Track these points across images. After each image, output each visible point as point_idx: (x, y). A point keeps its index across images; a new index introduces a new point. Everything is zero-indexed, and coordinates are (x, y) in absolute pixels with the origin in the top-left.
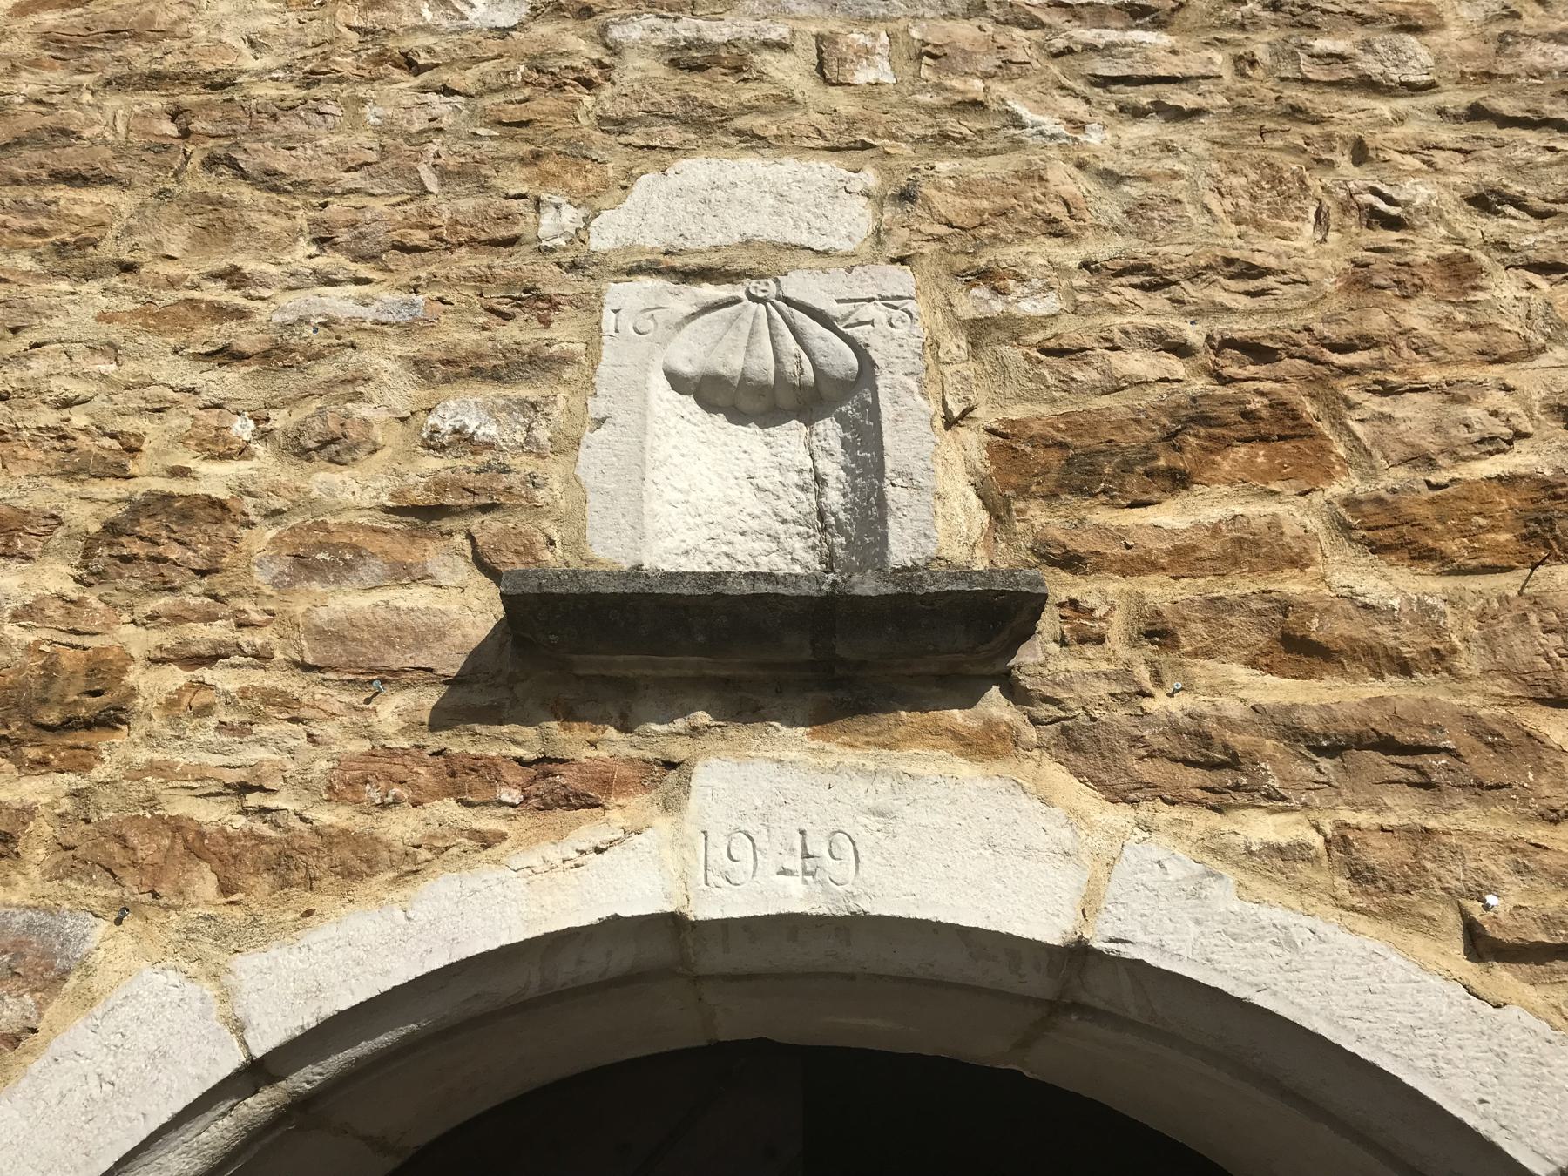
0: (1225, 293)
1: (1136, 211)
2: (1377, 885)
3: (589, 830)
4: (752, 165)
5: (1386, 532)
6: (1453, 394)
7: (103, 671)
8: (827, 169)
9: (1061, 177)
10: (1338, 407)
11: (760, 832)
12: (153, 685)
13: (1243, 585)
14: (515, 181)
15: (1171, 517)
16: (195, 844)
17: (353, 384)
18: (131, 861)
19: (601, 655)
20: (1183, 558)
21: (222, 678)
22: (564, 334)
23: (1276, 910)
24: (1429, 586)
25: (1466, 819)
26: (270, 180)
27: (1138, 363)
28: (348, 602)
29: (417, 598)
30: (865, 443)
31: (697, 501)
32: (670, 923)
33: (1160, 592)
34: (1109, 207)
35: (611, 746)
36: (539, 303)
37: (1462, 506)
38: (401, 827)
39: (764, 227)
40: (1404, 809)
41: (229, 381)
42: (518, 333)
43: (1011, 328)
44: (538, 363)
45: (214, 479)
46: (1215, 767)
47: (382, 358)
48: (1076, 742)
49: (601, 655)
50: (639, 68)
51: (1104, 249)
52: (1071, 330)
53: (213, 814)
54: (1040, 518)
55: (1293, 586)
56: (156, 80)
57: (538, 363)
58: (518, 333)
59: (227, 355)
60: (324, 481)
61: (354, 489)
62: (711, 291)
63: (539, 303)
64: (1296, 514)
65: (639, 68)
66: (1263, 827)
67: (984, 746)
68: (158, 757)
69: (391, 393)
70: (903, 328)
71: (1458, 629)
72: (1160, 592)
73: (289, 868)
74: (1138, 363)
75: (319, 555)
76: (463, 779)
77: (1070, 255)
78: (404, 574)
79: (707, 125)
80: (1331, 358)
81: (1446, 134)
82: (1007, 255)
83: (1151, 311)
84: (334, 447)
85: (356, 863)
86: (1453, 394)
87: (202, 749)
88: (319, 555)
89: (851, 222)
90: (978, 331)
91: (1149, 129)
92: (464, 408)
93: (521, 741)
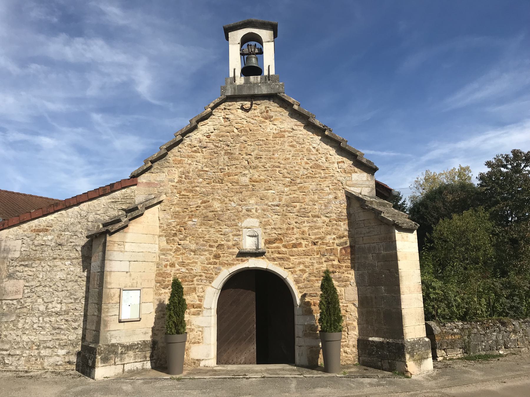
0: (279, 230)
1: (275, 224)
2: (280, 265)
3: (244, 263)
4: (252, 219)
5: (285, 246)
6: (291, 237)
7: (219, 254)
8: (256, 220)
9: (271, 221)
10: (284, 238)
11: (252, 263)
12: (222, 255)
13: (277, 250)
14: (237, 221)
15: (274, 245)
16: (226, 264)
17: (229, 236)
18: (223, 264)
19: (243, 255)
20: (274, 248)
21: (225, 255)
22: (241, 233)
23: (276, 267)
24: (286, 249)
25: (286, 262)
26: (221, 221)
27: (273, 235)
28: (231, 250)
29: (234, 250)
30: (258, 240)
31: (249, 244)
32: (231, 291)
33: (273, 250)
34: (273, 223)
35: (245, 258)
36: (239, 231)
37: (289, 245)
38: (235, 263)
39: (253, 225)
40: (283, 262)
41: (222, 236)
42: (238, 233)
43: (266, 232)
44: (239, 235)
45: (222, 243)
46: (274, 259)
47: (230, 234)
48: (268, 258)
49: (243, 255)
50: (244, 211)
51: (272, 227)
52: (270, 233)
53: (226, 262)
54: (267, 245)
55: (279, 250)
56: (213, 211)
57: (239, 235)
58: (238, 233)
59: (222, 234)
60: (228, 243)
61: (230, 243)
62: (249, 229)
63: (239, 231)
64: (280, 245)
65: (244, 211)
66: (276, 263)
67: (263, 259)
68: (301, 260)
69: (231, 237)
70: (260, 231)
71: (288, 252)
72: (273, 250)
73: (230, 265)
74: (273, 235)
75: (229, 248)
76: (238, 260)
77: (270, 227)
78: (234, 249)
79: (248, 216)
80: (284, 235)
81: (295, 217)
82: (267, 227)
83: (275, 231)
84: (229, 241)
85: (233, 264)
86: (291, 237)
87: (225, 258)
88: (229, 248)
89: (257, 224)
90: (265, 233)
91: (277, 216)
92: (235, 238)
93: (240, 258)
